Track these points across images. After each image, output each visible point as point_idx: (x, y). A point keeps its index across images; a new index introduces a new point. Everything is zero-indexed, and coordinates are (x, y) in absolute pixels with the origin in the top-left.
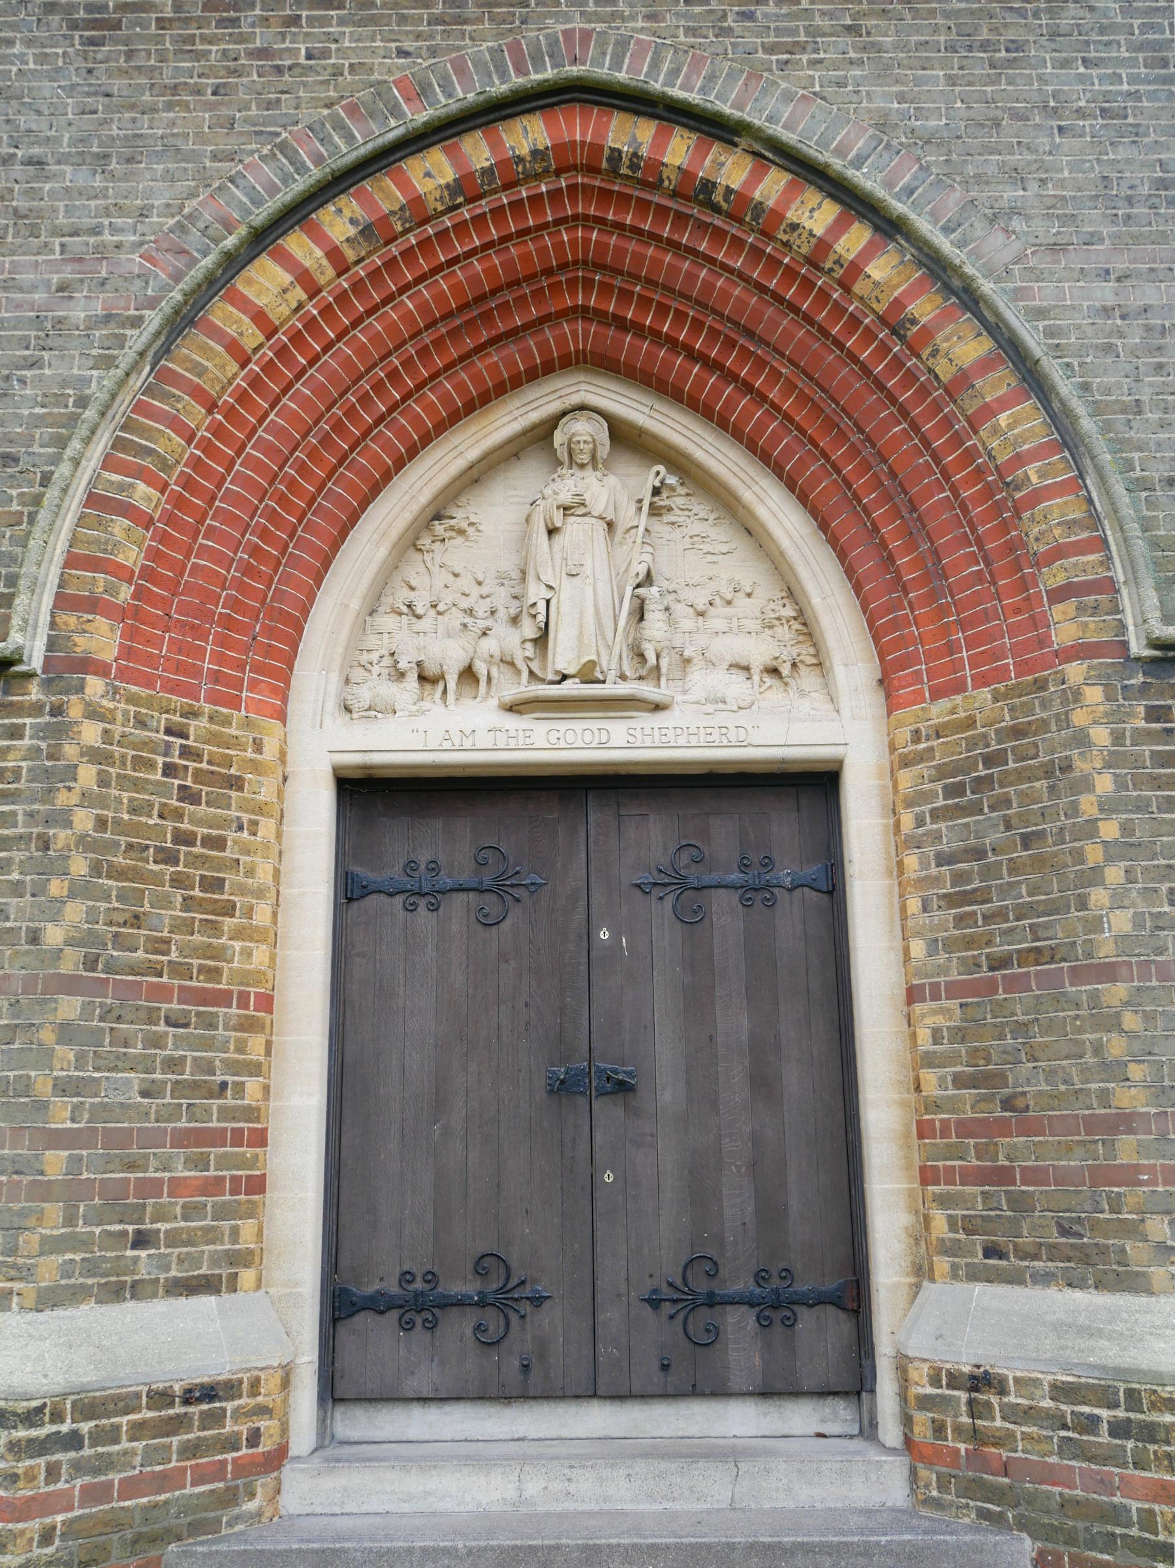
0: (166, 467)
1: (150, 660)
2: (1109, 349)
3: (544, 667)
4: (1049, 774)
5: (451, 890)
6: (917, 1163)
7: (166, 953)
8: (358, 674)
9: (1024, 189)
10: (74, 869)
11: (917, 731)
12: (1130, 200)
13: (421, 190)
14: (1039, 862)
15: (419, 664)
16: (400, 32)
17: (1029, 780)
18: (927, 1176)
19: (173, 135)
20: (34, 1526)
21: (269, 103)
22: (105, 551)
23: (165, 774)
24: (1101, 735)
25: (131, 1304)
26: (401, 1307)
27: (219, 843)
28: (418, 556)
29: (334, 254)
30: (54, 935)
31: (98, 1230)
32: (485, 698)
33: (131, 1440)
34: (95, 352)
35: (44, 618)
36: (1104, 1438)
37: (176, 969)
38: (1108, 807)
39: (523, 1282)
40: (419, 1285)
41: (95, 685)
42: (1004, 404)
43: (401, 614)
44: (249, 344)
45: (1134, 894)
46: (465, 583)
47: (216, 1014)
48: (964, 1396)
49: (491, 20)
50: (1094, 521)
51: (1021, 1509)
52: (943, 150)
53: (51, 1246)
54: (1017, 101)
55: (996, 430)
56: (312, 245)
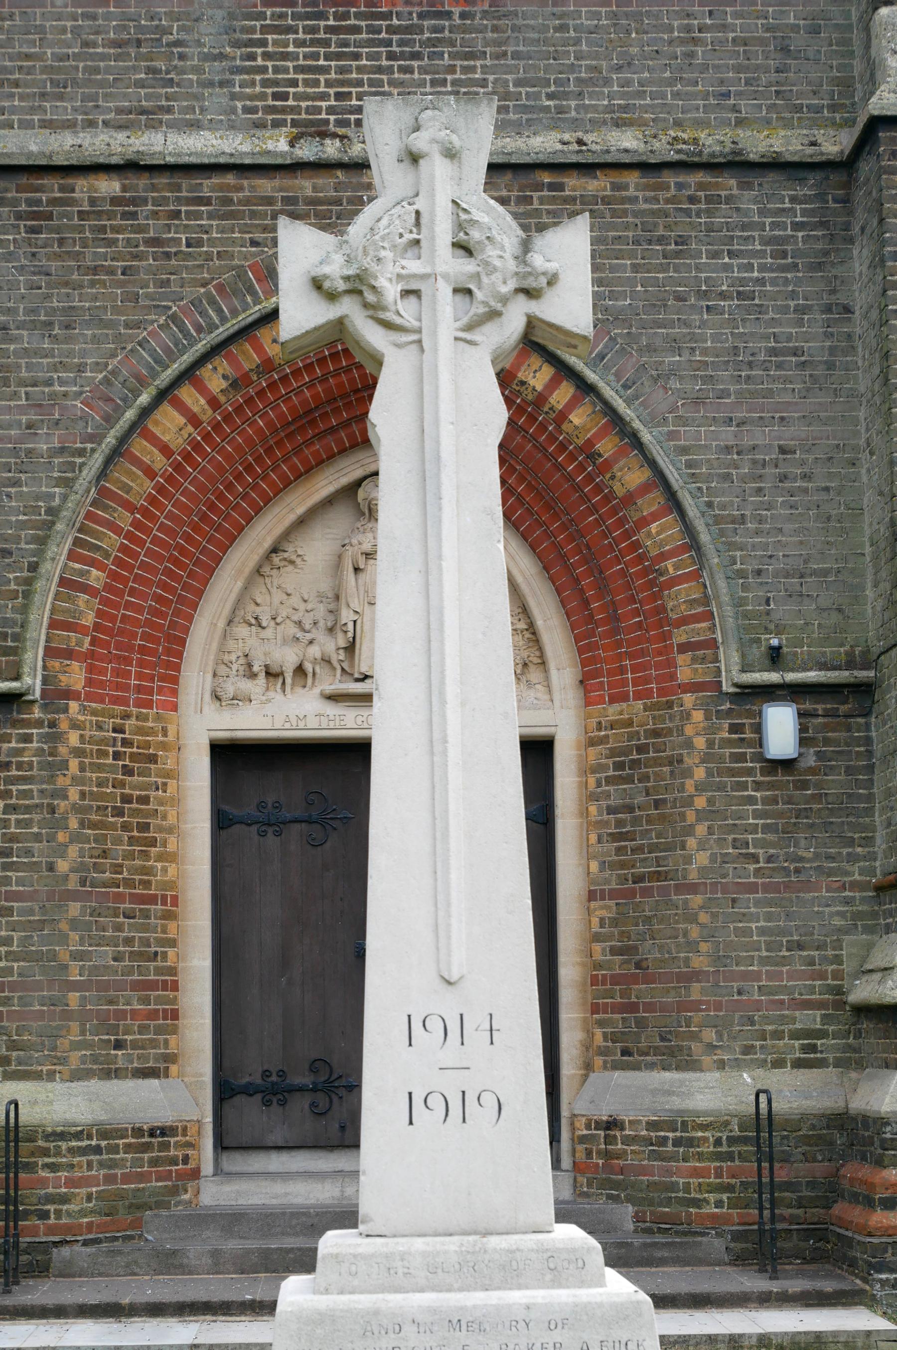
0: (107, 555)
1: (102, 684)
2: (727, 477)
3: (352, 665)
4: (671, 763)
5: (290, 822)
6: (590, 1000)
7: (121, 873)
8: (222, 670)
9: (680, 355)
10: (71, 825)
11: (600, 723)
12: (750, 365)
13: (270, 353)
14: (663, 818)
15: (266, 666)
16: (252, 225)
17: (660, 765)
18: (595, 1009)
19: (97, 307)
20: (83, 1191)
21: (162, 282)
22: (74, 617)
23: (114, 759)
24: (700, 742)
25: (115, 1081)
26: (262, 1092)
27: (145, 800)
28: (261, 580)
29: (214, 403)
30: (63, 866)
31: (96, 1038)
32: (311, 689)
33: (125, 1153)
34: (56, 475)
35: (40, 663)
36: (670, 1148)
37: (129, 883)
38: (700, 788)
39: (341, 1077)
40: (274, 1078)
41: (74, 706)
42: (655, 517)
43: (251, 625)
44: (157, 467)
45: (712, 842)
46: (295, 601)
47: (149, 910)
48: (602, 1133)
49: (316, 215)
50: (706, 600)
51: (628, 1191)
52: (627, 325)
53: (76, 1046)
54: (680, 286)
55: (649, 534)
56: (198, 395)
